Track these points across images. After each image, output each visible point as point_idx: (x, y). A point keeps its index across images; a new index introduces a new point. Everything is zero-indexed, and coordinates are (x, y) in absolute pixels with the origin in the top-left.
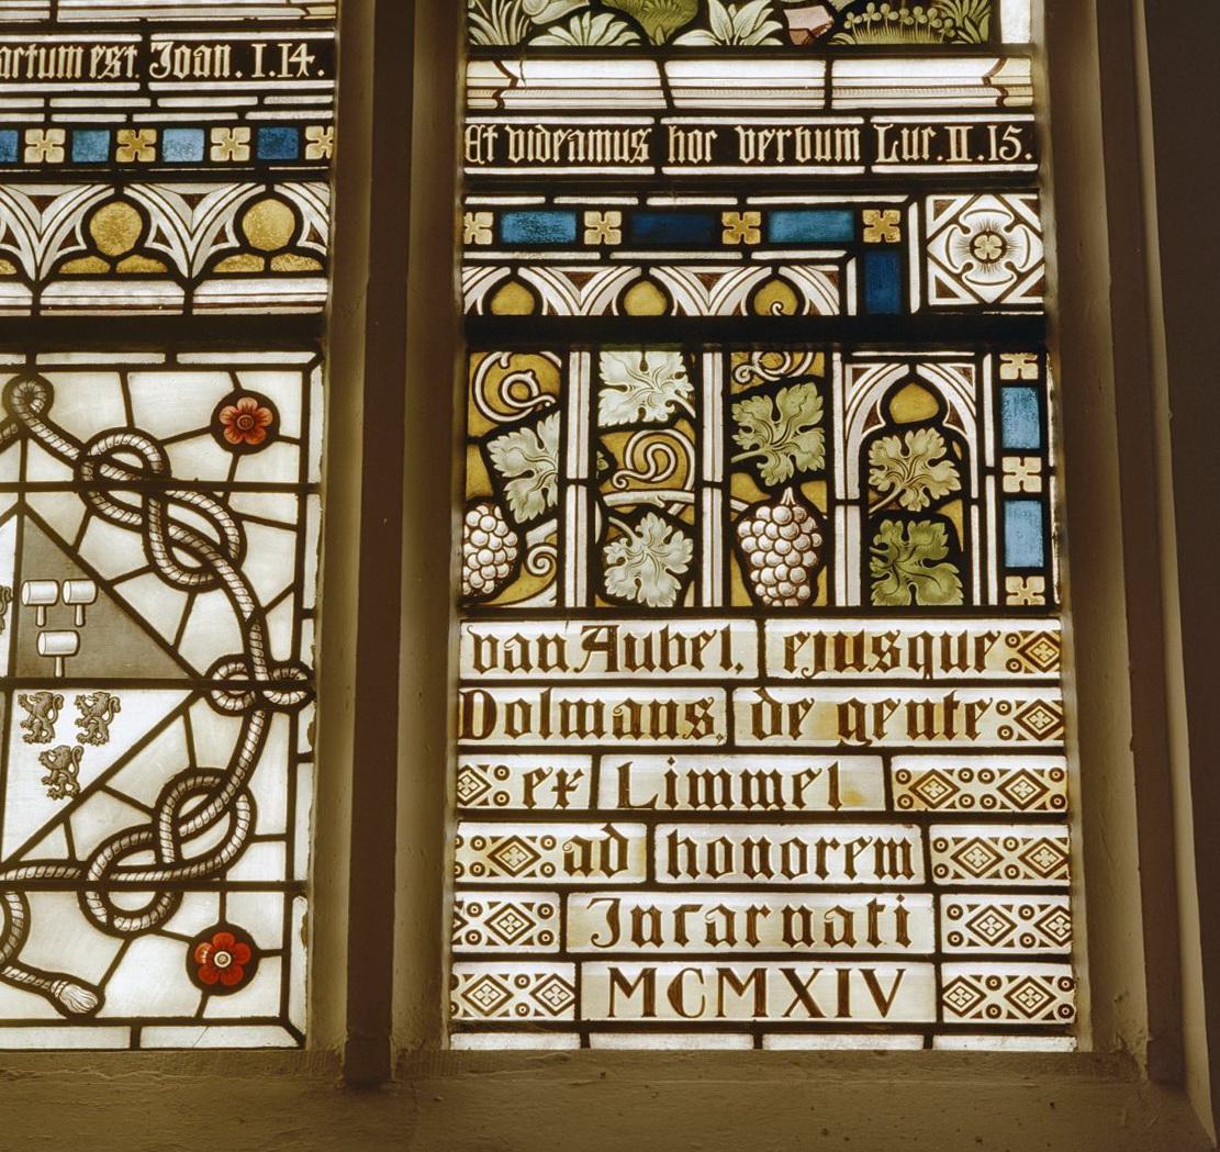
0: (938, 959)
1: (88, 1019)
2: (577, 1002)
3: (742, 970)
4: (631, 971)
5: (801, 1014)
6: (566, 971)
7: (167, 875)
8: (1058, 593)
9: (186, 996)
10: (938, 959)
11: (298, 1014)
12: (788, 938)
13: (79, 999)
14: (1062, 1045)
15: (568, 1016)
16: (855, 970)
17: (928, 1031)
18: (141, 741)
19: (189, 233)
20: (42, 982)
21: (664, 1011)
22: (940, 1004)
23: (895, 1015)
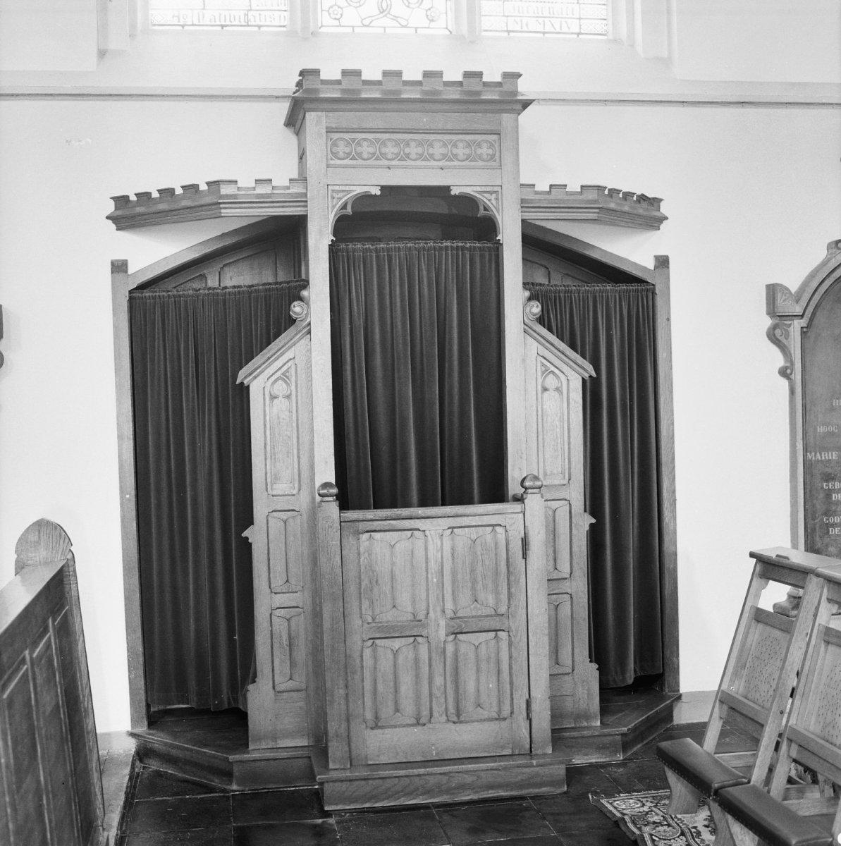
0: (580, 19)
1: (405, 27)
2: (507, 26)
3: (541, 20)
4: (518, 19)
5: (552, 30)
6: (505, 19)
7: (49, 841)
8: (30, 697)
9: (426, 23)
10: (580, 19)
11: (323, 30)
12: (550, 13)
13: (404, 23)
14: (284, 29)
15: (505, 29)
16: (563, 20)
17: (578, 34)
18: (791, 440)
19: (338, 26)
20: (395, 18)
21: (525, 29)
22: (580, 28)
23: (571, 31)
